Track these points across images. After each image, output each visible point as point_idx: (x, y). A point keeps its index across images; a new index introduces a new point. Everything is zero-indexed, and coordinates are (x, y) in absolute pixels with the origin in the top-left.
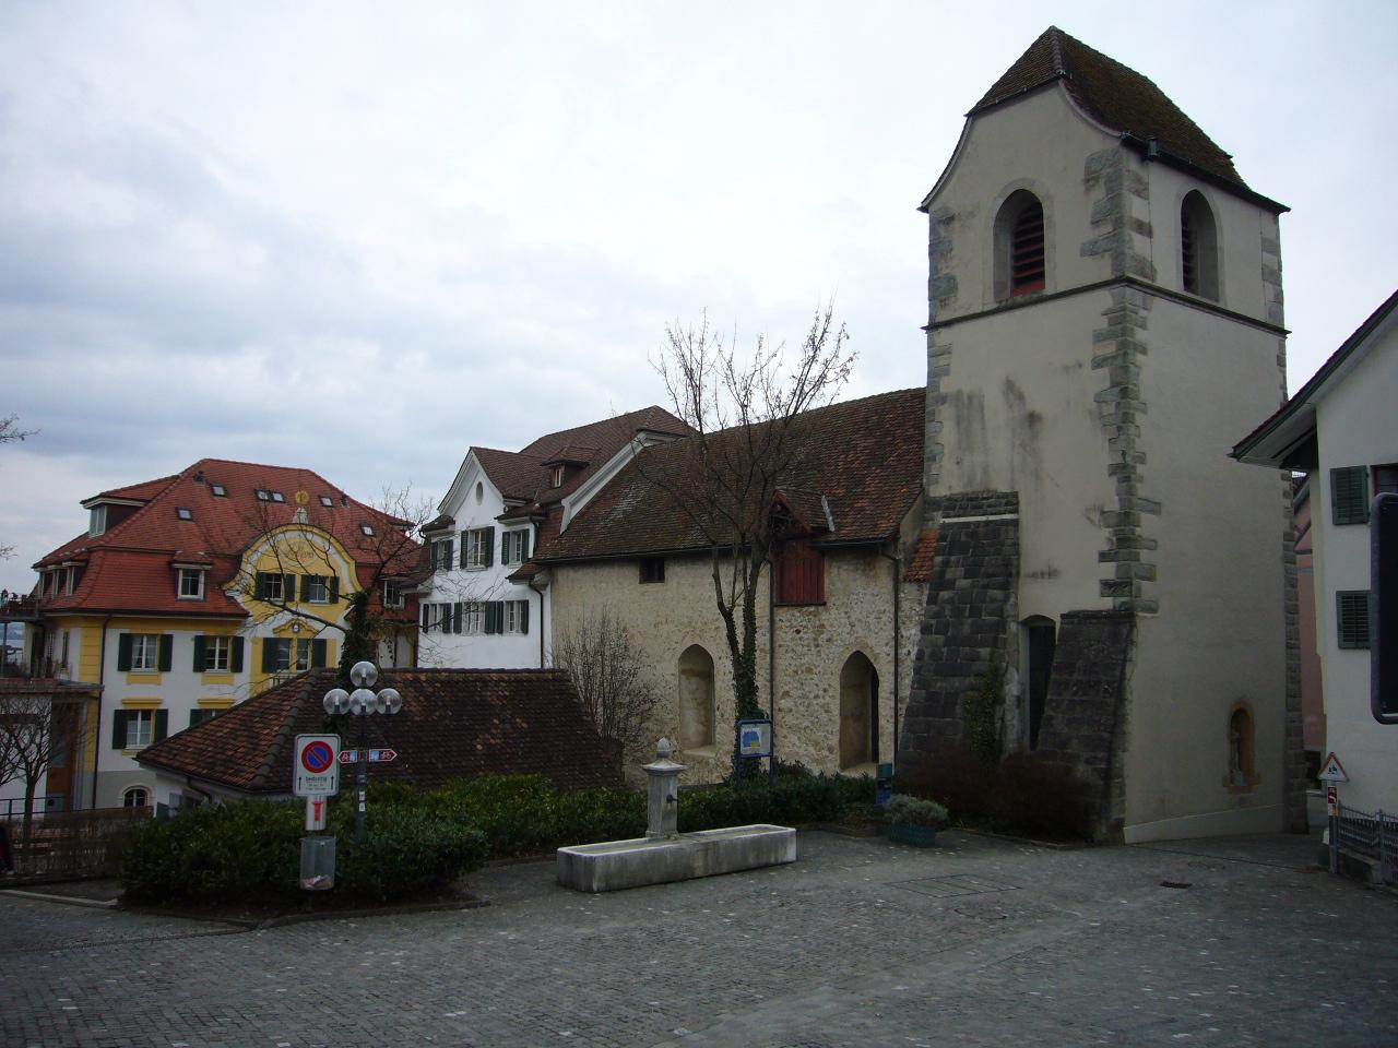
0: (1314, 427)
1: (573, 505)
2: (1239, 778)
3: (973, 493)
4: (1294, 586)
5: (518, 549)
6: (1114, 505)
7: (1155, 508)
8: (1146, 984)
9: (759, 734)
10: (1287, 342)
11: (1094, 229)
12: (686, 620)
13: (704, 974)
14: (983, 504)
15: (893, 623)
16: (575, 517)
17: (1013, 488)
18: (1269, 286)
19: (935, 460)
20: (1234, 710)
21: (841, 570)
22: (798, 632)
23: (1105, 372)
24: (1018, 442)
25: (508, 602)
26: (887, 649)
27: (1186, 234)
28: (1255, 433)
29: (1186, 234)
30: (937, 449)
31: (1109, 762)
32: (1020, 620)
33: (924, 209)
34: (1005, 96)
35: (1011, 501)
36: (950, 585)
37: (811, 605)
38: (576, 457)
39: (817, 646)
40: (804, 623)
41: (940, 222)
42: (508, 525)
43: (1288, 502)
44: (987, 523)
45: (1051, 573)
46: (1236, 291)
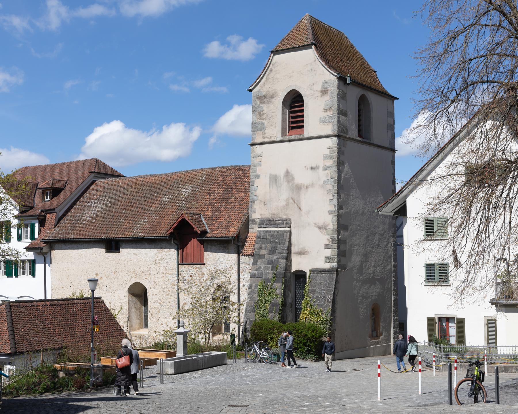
1: (60, 211)
10: (396, 155)
12: (132, 270)
23: (328, 171)
30: (255, 198)
38: (57, 185)
44: (278, 231)
46: (377, 135)
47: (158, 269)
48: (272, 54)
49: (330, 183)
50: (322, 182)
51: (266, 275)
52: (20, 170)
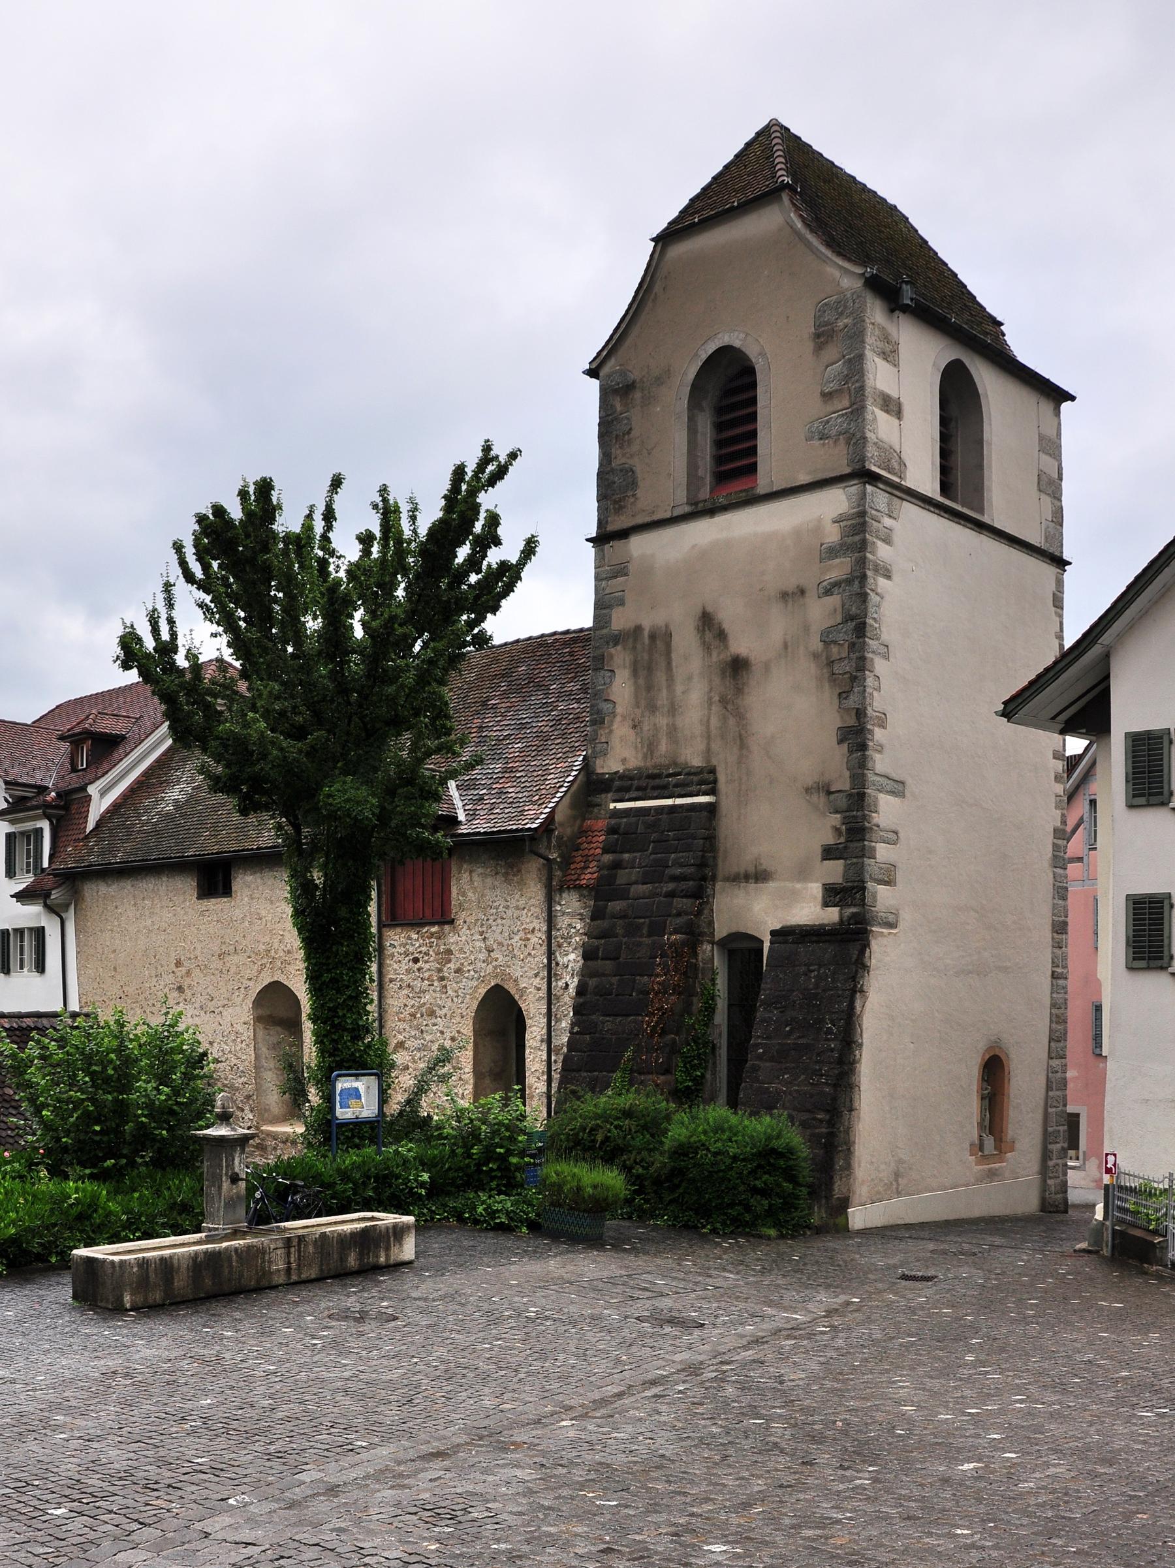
0: (1107, 677)
1: (103, 793)
2: (989, 1142)
3: (655, 767)
4: (1064, 898)
5: (28, 857)
6: (843, 783)
7: (898, 788)
8: (905, 1402)
9: (362, 1091)
11: (825, 402)
12: (262, 947)
13: (280, 1415)
14: (669, 783)
15: (545, 948)
16: (107, 811)
17: (708, 761)
18: (1047, 500)
19: (603, 723)
20: (987, 1057)
21: (475, 877)
22: (416, 960)
23: (834, 601)
24: (717, 698)
25: (15, 930)
26: (536, 982)
27: (944, 421)
28: (1032, 683)
29: (945, 422)
31: (831, 1123)
32: (716, 939)
33: (592, 373)
34: (707, 213)
35: (706, 779)
36: (623, 894)
37: (433, 924)
38: (106, 726)
39: (442, 979)
40: (424, 949)
41: (616, 392)
42: (12, 822)
43: (1059, 789)
45: (760, 876)
46: (1006, 500)
48: (660, 245)
52: (849, 1149)
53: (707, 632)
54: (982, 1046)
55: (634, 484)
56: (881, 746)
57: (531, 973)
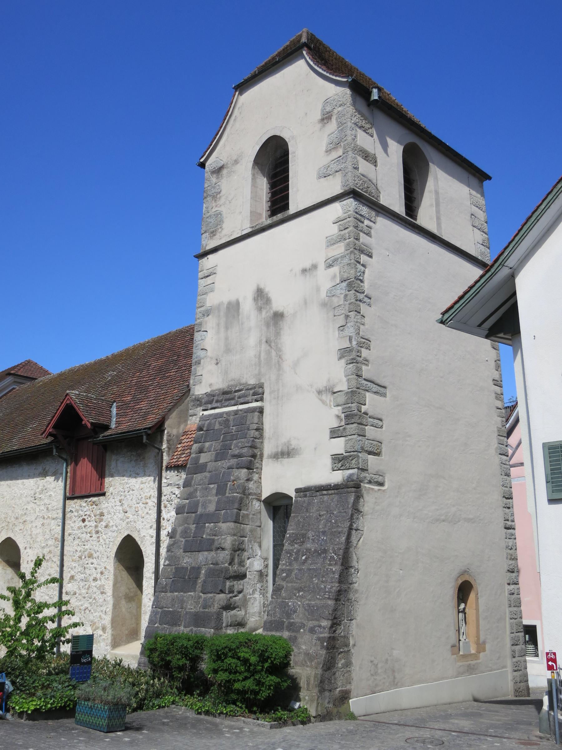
22: (84, 521)
23: (335, 270)
30: (202, 354)
32: (263, 498)
39: (97, 532)
40: (88, 513)
44: (236, 412)
47: (37, 510)
49: (338, 292)
50: (323, 295)
51: (204, 506)
53: (259, 300)
54: (455, 574)
55: (221, 221)
56: (367, 361)
57: (148, 526)
